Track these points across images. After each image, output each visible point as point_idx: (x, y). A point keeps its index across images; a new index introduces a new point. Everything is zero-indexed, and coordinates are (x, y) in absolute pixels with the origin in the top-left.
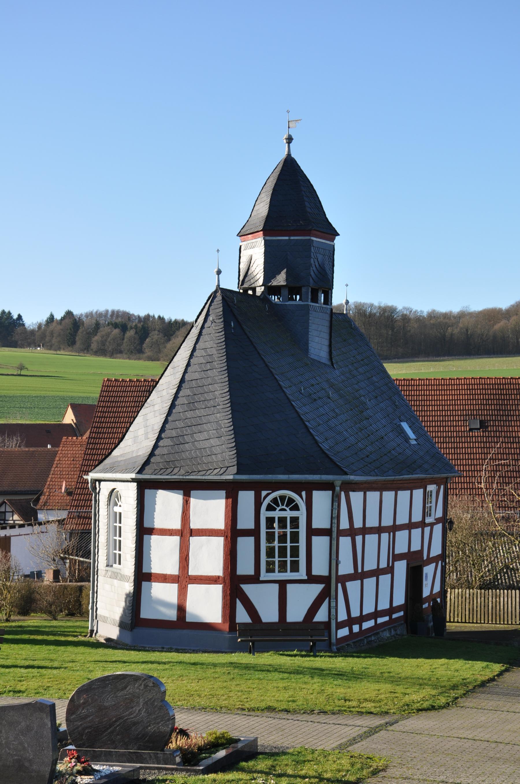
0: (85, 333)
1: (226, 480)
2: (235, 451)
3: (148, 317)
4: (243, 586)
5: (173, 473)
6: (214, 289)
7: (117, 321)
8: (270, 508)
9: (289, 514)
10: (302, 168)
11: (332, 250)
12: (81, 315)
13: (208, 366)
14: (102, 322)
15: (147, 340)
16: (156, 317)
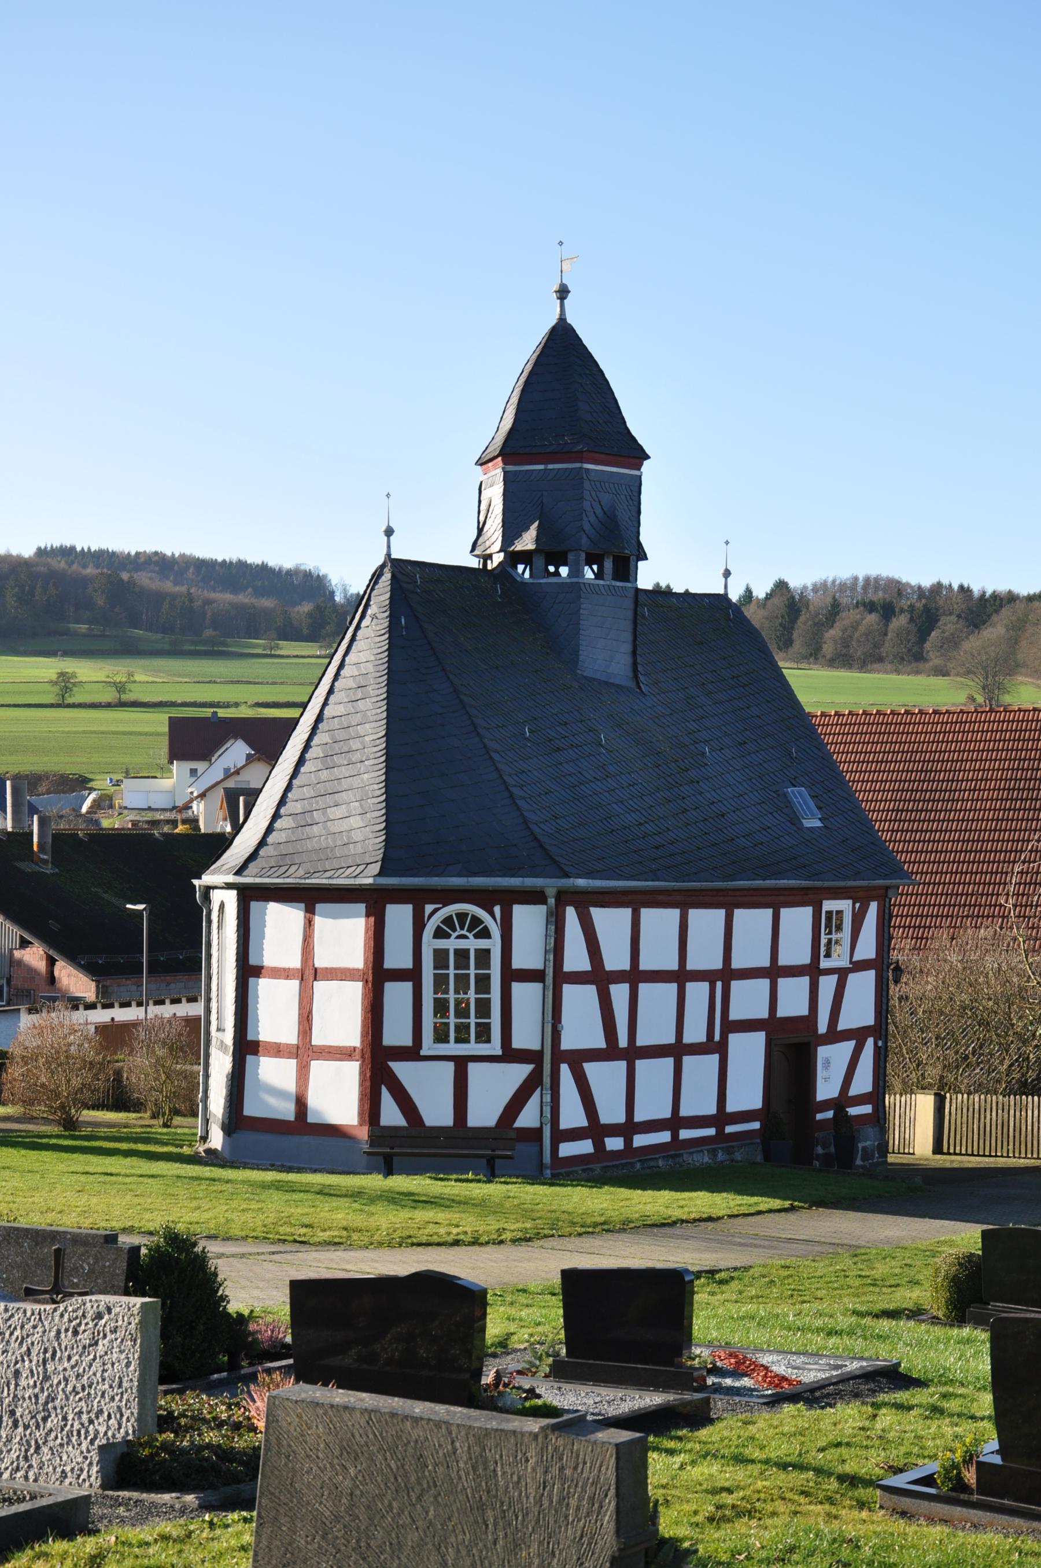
0: (810, 623)
1: (360, 885)
2: (384, 837)
3: (938, 587)
5: (287, 874)
6: (381, 562)
7: (875, 599)
9: (473, 944)
10: (585, 342)
11: (637, 484)
12: (805, 587)
13: (359, 695)
14: (844, 601)
15: (933, 634)
16: (955, 587)
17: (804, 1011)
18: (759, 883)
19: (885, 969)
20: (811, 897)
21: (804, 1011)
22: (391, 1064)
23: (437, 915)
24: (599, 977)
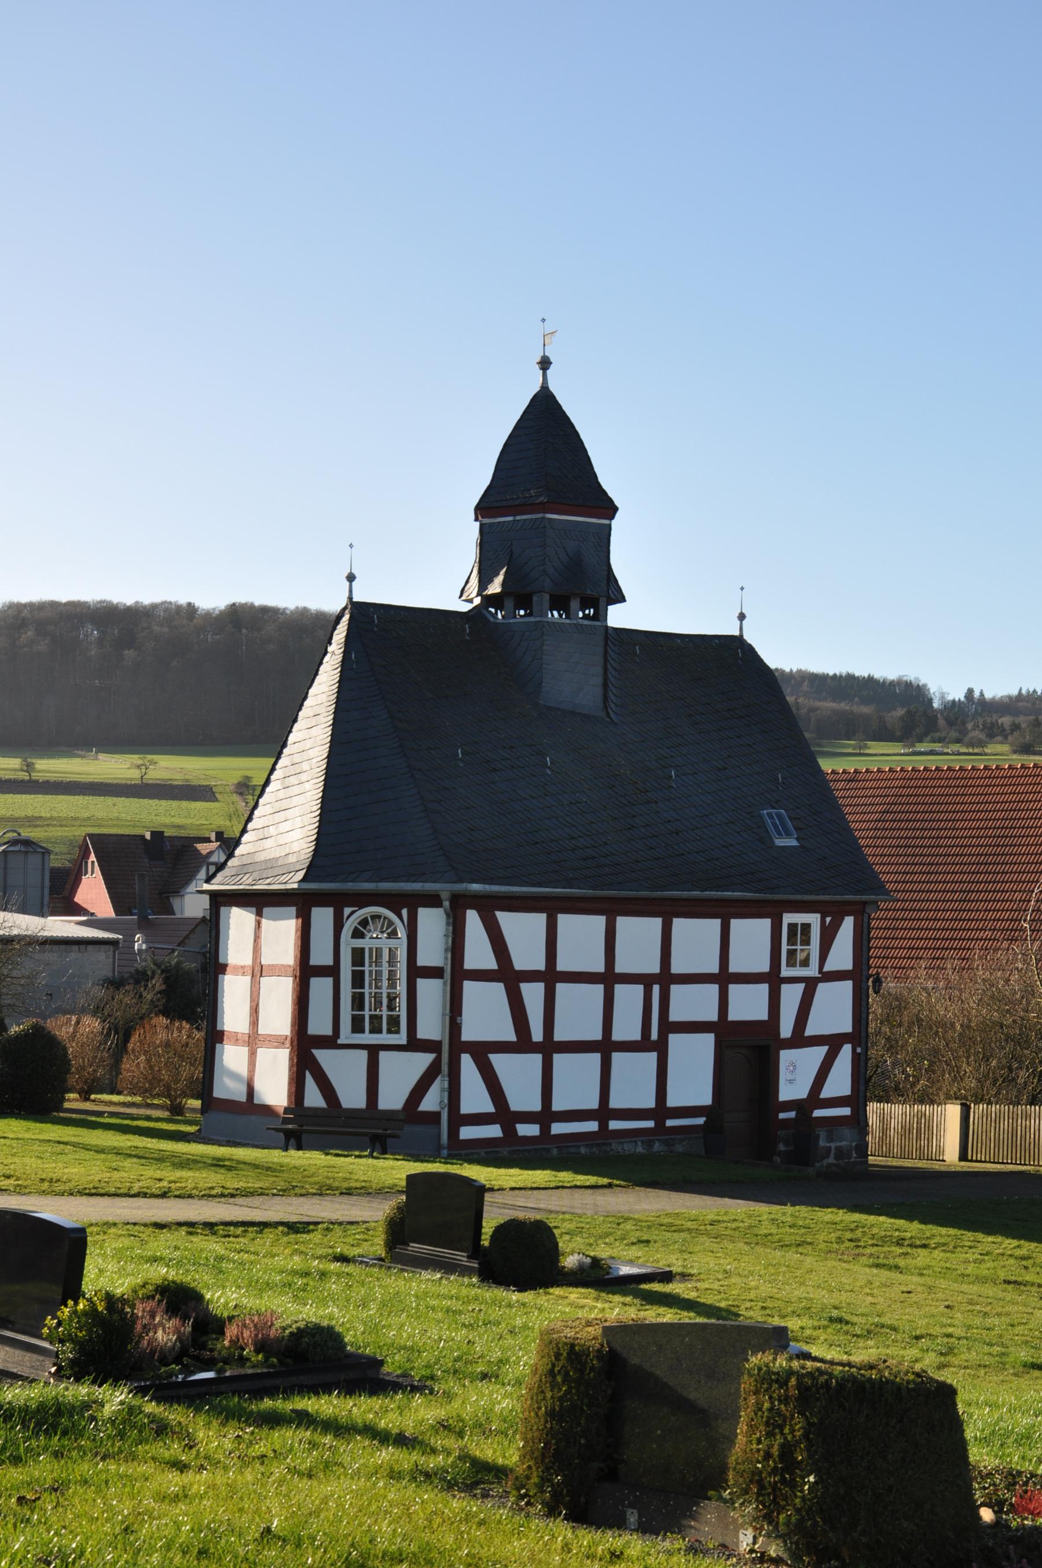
6: (343, 605)
8: (357, 934)
10: (564, 408)
17: (763, 1015)
19: (861, 977)
20: (772, 910)
21: (763, 1015)
24: (507, 975)
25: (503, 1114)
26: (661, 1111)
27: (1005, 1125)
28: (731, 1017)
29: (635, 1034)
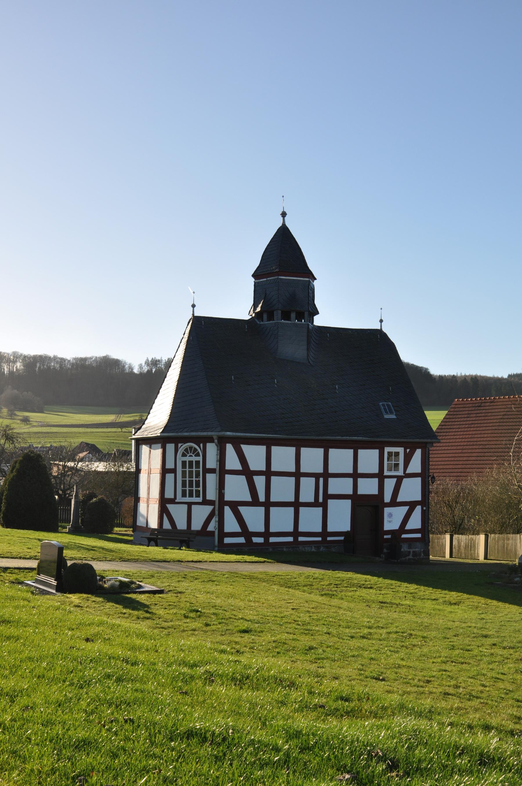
4: (168, 505)
8: (184, 455)
9: (194, 459)
18: (348, 438)
19: (426, 476)
20: (380, 446)
22: (167, 505)
23: (182, 447)
24: (246, 472)
25: (245, 532)
26: (324, 533)
27: (501, 543)
28: (359, 492)
29: (311, 499)
